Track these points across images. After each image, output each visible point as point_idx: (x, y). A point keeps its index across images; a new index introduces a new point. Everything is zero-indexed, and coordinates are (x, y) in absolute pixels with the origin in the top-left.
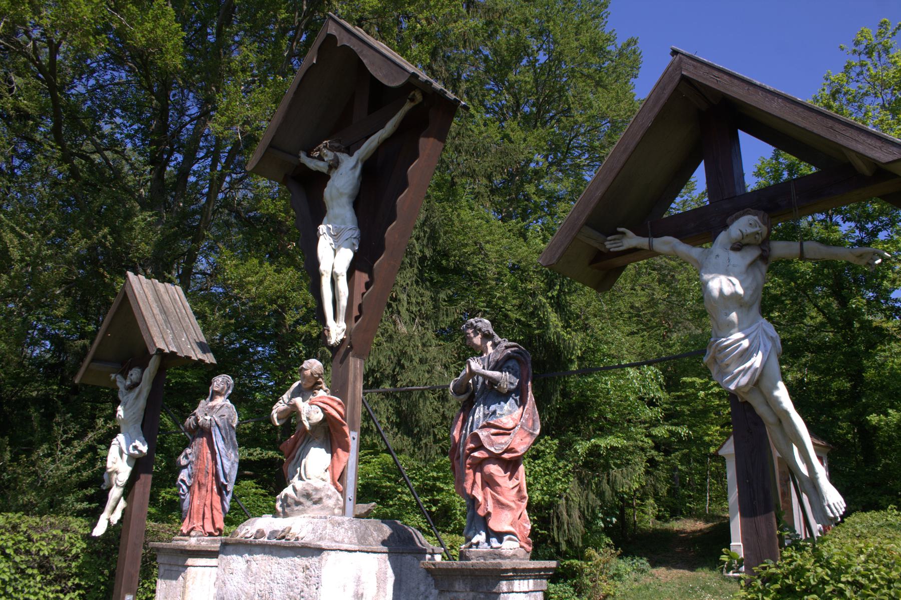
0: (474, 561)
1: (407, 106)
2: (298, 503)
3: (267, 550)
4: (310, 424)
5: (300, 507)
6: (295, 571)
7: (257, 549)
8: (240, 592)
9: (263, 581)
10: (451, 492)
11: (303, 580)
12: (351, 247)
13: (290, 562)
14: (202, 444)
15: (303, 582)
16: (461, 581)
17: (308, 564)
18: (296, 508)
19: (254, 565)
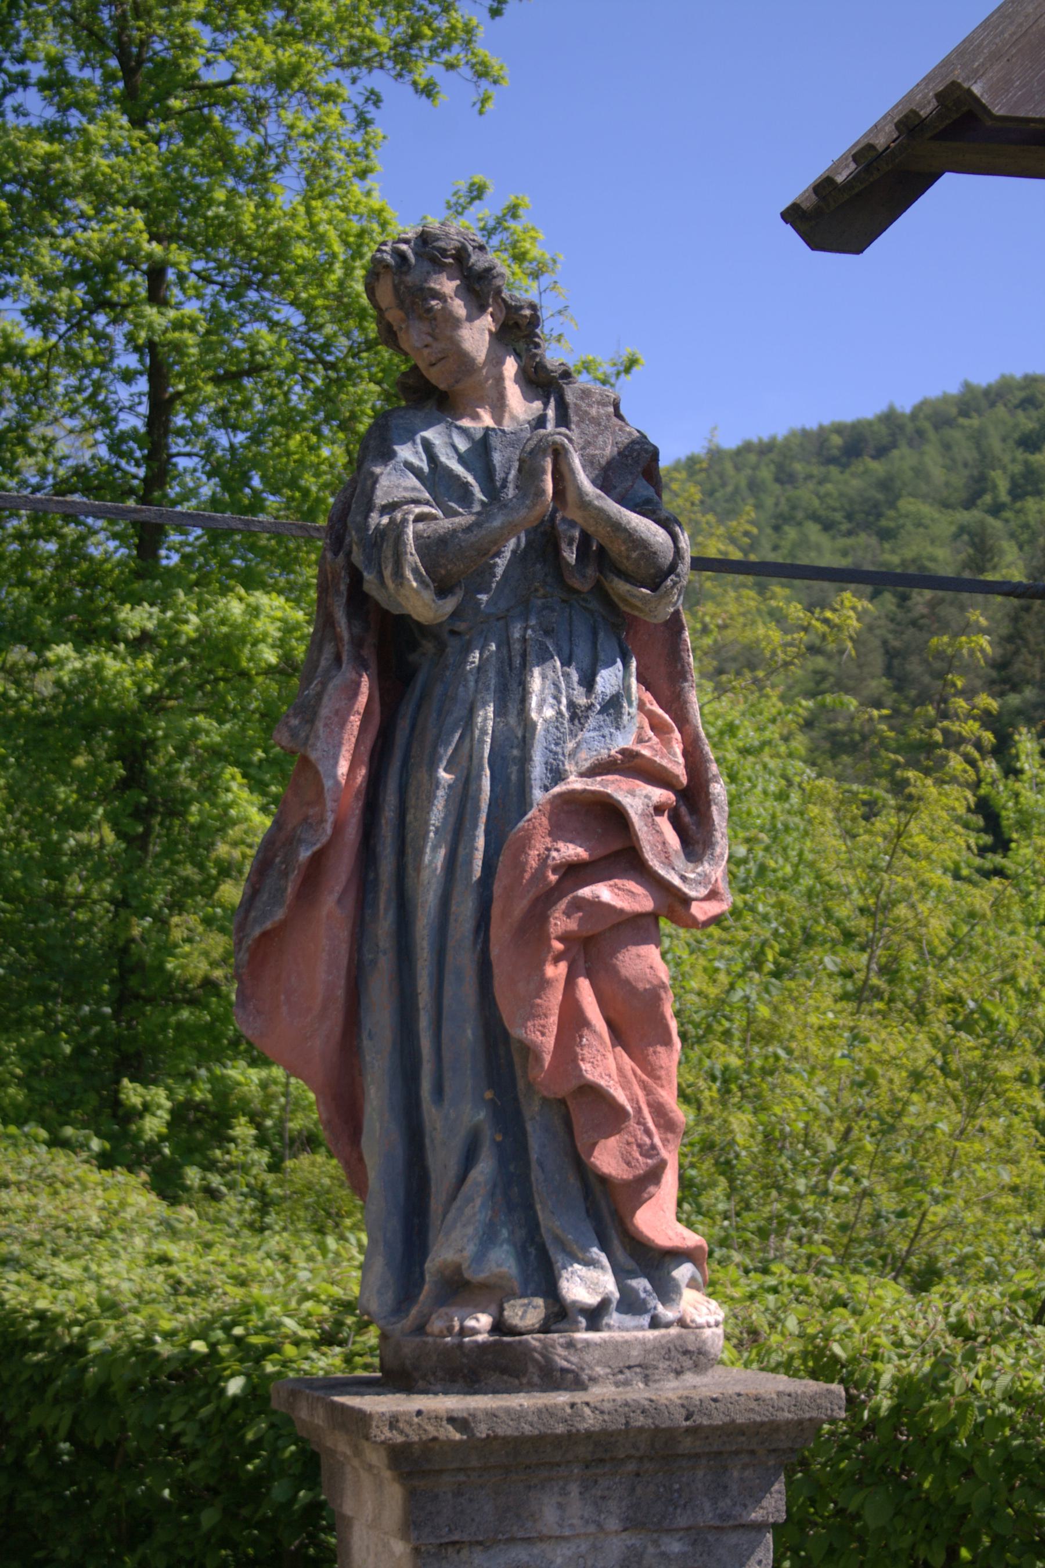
0: (602, 1392)
16: (574, 1489)
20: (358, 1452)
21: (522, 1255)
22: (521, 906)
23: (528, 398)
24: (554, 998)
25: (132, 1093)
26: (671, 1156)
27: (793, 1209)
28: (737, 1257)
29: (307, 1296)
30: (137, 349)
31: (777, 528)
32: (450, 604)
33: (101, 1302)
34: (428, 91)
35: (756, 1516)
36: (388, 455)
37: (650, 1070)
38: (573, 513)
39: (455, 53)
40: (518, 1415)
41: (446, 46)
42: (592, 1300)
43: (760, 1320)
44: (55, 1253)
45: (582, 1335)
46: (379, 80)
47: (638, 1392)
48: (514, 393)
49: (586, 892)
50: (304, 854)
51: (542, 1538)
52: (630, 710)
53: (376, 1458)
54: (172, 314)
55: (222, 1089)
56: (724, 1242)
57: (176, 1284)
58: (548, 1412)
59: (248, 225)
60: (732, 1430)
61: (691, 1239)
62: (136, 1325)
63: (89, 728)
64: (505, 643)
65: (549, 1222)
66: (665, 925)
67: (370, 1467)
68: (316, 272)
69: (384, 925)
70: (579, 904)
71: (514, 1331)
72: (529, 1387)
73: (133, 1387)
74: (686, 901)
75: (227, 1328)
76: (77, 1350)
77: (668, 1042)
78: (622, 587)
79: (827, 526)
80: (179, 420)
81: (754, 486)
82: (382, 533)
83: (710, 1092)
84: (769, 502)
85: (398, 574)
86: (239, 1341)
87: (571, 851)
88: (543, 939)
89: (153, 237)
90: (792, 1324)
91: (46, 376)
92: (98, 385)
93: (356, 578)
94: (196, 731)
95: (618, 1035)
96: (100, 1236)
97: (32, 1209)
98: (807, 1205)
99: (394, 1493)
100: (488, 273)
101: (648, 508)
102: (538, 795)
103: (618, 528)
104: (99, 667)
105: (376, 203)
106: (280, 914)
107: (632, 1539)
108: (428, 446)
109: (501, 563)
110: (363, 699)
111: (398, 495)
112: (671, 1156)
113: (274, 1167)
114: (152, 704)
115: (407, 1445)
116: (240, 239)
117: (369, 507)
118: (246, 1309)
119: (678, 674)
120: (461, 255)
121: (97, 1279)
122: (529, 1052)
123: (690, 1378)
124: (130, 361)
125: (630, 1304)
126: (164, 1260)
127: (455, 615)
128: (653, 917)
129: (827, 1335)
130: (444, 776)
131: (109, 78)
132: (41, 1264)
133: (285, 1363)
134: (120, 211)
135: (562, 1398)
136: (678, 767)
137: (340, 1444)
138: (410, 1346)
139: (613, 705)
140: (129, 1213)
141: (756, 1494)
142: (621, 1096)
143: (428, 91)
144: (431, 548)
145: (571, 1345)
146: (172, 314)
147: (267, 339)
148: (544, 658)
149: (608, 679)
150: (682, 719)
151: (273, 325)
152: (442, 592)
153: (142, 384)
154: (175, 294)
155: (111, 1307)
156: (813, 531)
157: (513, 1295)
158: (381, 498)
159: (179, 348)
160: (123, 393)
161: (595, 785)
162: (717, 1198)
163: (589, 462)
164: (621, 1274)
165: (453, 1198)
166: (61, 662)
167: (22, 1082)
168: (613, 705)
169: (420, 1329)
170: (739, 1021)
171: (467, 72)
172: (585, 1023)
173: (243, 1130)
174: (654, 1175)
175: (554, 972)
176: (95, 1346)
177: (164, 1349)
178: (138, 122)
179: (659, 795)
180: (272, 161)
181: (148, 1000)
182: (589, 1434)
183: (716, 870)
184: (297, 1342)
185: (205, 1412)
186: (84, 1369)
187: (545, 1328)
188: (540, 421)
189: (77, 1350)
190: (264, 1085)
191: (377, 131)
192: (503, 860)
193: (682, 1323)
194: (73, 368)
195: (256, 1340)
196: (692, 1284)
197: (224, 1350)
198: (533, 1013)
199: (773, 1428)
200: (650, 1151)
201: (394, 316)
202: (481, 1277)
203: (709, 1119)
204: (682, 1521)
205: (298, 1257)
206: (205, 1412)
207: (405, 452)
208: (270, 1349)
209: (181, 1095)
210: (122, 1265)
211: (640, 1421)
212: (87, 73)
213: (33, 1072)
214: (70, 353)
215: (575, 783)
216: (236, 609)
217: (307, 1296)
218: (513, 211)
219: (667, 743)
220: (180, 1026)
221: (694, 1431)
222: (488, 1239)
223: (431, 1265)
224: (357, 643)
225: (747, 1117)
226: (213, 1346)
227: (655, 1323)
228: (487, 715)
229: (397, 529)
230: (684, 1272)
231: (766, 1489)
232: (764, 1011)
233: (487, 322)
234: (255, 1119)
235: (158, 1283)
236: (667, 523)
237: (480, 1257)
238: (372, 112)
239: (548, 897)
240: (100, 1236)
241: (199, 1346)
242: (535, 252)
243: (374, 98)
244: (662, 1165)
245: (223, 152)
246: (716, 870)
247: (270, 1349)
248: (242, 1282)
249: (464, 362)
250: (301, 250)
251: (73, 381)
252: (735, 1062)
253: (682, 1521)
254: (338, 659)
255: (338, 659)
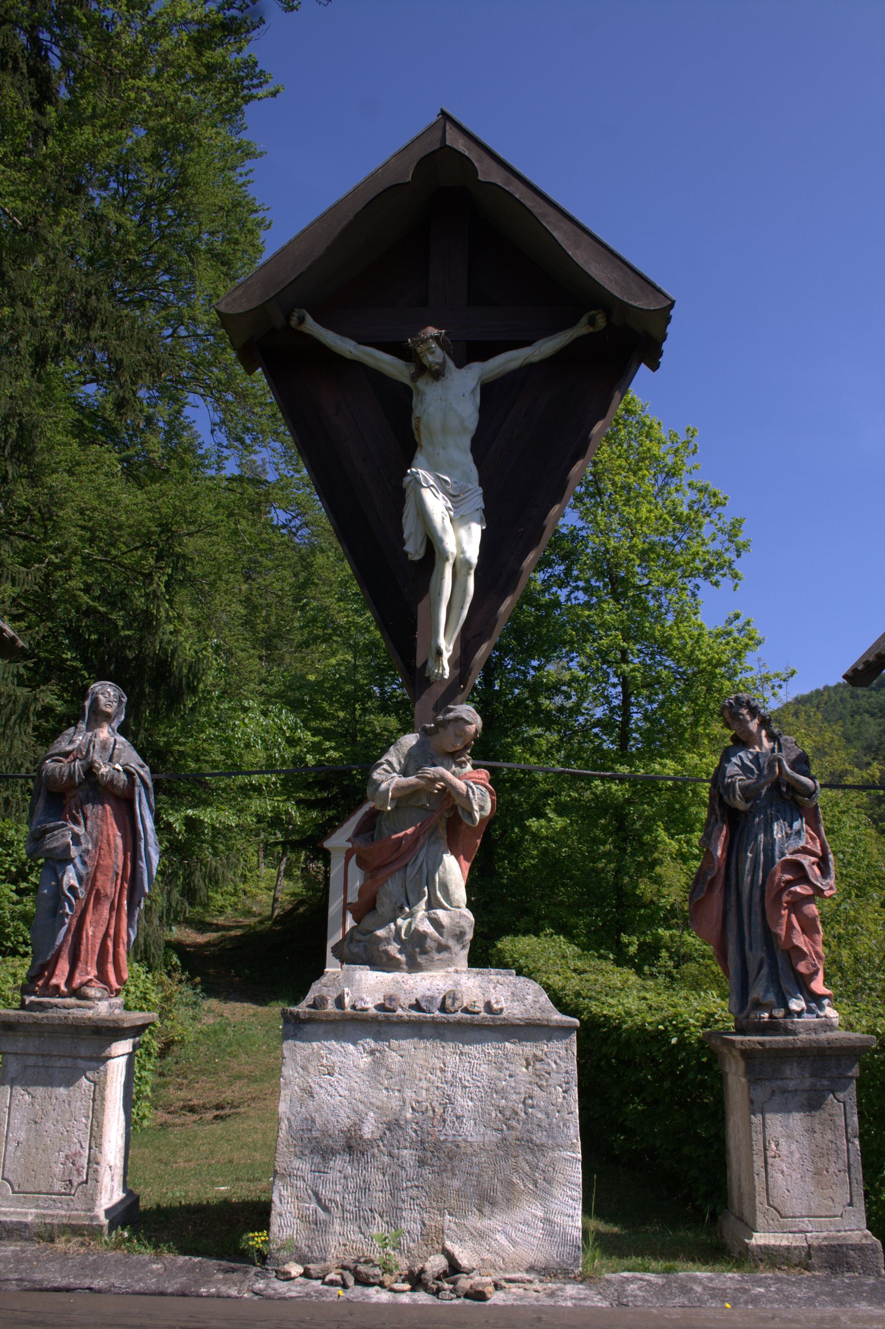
0: (803, 1036)
1: (581, 329)
2: (442, 948)
3: (427, 1030)
4: (481, 816)
5: (445, 955)
6: (506, 1065)
7: (321, 1029)
8: (361, 1106)
9: (424, 1084)
10: (258, 898)
11: (528, 1079)
12: (480, 523)
13: (492, 1052)
14: (104, 819)
15: (530, 1083)
16: (795, 1064)
17: (539, 1053)
18: (437, 956)
19: (394, 1059)
20: (730, 1052)
21: (777, 996)
22: (774, 893)
23: (769, 741)
24: (785, 920)
25: (625, 938)
26: (821, 967)
27: (865, 984)
28: (845, 1001)
29: (697, 1011)
30: (618, 676)
31: (852, 716)
32: (749, 805)
33: (625, 1012)
34: (716, 584)
35: (850, 1074)
36: (729, 761)
37: (813, 941)
38: (785, 778)
39: (725, 570)
40: (778, 1042)
41: (722, 568)
42: (798, 1009)
43: (852, 1019)
44: (607, 995)
45: (796, 1020)
46: (699, 581)
47: (813, 1036)
48: (765, 740)
49: (793, 889)
50: (709, 878)
51: (786, 1078)
52: (804, 834)
53: (736, 1053)
54: (631, 666)
55: (658, 939)
56: (841, 996)
57: (650, 1007)
58: (787, 1041)
59: (657, 634)
60: (842, 1048)
61: (828, 992)
62: (638, 1019)
63: (606, 811)
64: (766, 815)
65: (785, 986)
66: (817, 898)
67: (734, 1057)
68: (682, 649)
69: (733, 898)
70: (791, 893)
71: (775, 1018)
72: (781, 1035)
73: (638, 1041)
74: (823, 891)
75: (670, 1022)
76: (618, 1028)
77: (818, 933)
78: (800, 798)
79: (872, 715)
80: (633, 699)
81: (842, 700)
82: (729, 784)
83: (833, 943)
84: (849, 706)
85: (734, 797)
86: (674, 1026)
87: (788, 877)
88: (781, 903)
89: (624, 641)
90: (864, 1023)
91: (586, 687)
92: (604, 689)
93: (721, 797)
94: (644, 810)
95: (804, 931)
96: (621, 990)
97: (596, 980)
98: (869, 982)
99: (742, 1065)
100: (756, 708)
101: (806, 774)
102: (777, 860)
103: (798, 781)
104: (610, 788)
105: (699, 621)
106: (702, 895)
107: (813, 1080)
108: (740, 757)
109: (764, 792)
110: (724, 832)
111: (733, 773)
112: (821, 967)
113: (676, 967)
114: (628, 802)
115: (746, 1050)
116: (655, 638)
117: (724, 777)
118: (676, 1015)
119: (817, 821)
120: (748, 702)
121: (623, 1004)
122: (778, 936)
123: (829, 1033)
124: (615, 680)
125: (810, 1011)
126: (645, 998)
127: (751, 807)
128: (813, 895)
129: (875, 1026)
130: (749, 855)
131: (605, 586)
132: (603, 999)
133: (691, 1033)
134: (613, 633)
135: (791, 1038)
136: (818, 850)
137: (725, 1050)
138: (744, 1022)
139: (798, 833)
140: (630, 982)
141: (850, 1068)
142: (805, 949)
143: (716, 584)
144: (744, 789)
145: (793, 1022)
146: (631, 666)
147: (665, 673)
148: (777, 820)
149: (796, 825)
150: (819, 835)
151: (666, 667)
152: (747, 801)
153: (619, 689)
154: (631, 657)
155: (629, 1013)
156: (866, 716)
157: (774, 1007)
158: (728, 774)
159: (634, 678)
160: (613, 691)
161: (794, 857)
162: (837, 980)
163: (788, 761)
164: (807, 1002)
165: (756, 978)
166: (596, 787)
167: (586, 936)
168: (798, 833)
169: (747, 1017)
170: (844, 916)
171: (729, 576)
172: (793, 927)
173: (664, 954)
174: (816, 973)
175: (785, 912)
176: (625, 1026)
177: (649, 1028)
178: (617, 601)
179: (813, 859)
180: (663, 610)
181: (628, 906)
182: (799, 1048)
183: (832, 881)
184: (695, 1026)
185: (664, 1049)
186: (621, 1034)
187: (785, 1017)
188: (773, 750)
189: (618, 1028)
190: (671, 936)
191: (700, 598)
192: (768, 880)
193: (826, 1017)
194: (595, 684)
195: (681, 1026)
196: (829, 1005)
197: (670, 1029)
198: (778, 924)
199: (854, 1048)
200: (814, 965)
201: (729, 720)
202: (765, 1001)
203: (834, 952)
204: (828, 1075)
205: (691, 998)
206: (664, 1049)
207: (734, 760)
208: (685, 1029)
209: (642, 939)
210: (631, 1000)
211: (814, 1045)
212: (598, 584)
213: (589, 932)
214: (595, 679)
215: (788, 857)
216: (657, 767)
217: (697, 1011)
218: (748, 623)
219: (815, 843)
220: (640, 916)
221: (830, 1048)
222: (767, 991)
223: (750, 998)
224: (722, 816)
225: (847, 951)
226: (666, 1027)
227: (818, 1017)
228: (761, 837)
229: (733, 783)
230: (826, 1002)
231: (853, 1066)
232: (852, 913)
233: (756, 721)
234: (668, 949)
235: (644, 1007)
236: (813, 778)
237: (764, 996)
238: (697, 592)
239: (782, 890)
240: (621, 990)
241: (661, 1027)
242: (757, 636)
243: (697, 587)
244: (818, 970)
245: (646, 609)
246: (832, 881)
247: (685, 1029)
248: (673, 1007)
249: (750, 733)
250: (676, 642)
251: (595, 688)
252: (842, 931)
253: (828, 1075)
254: (716, 820)
255: (716, 820)
